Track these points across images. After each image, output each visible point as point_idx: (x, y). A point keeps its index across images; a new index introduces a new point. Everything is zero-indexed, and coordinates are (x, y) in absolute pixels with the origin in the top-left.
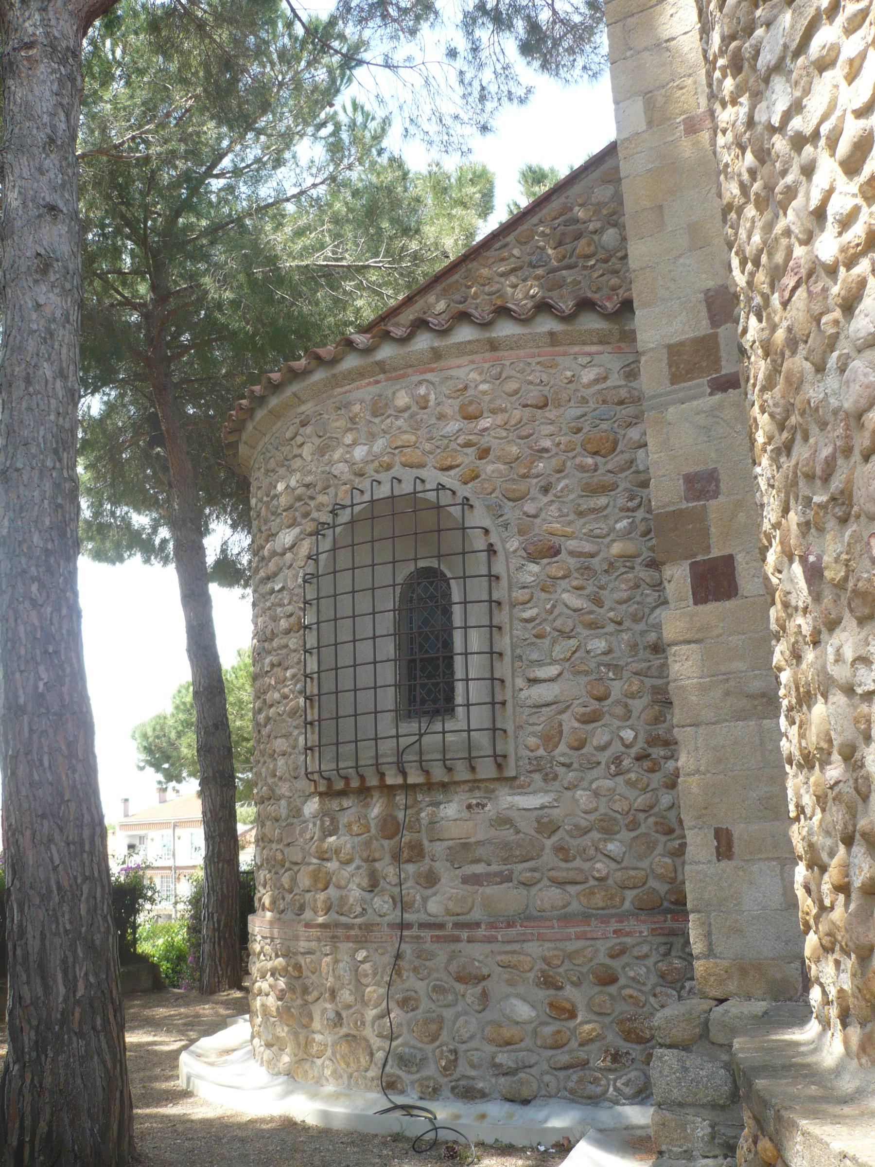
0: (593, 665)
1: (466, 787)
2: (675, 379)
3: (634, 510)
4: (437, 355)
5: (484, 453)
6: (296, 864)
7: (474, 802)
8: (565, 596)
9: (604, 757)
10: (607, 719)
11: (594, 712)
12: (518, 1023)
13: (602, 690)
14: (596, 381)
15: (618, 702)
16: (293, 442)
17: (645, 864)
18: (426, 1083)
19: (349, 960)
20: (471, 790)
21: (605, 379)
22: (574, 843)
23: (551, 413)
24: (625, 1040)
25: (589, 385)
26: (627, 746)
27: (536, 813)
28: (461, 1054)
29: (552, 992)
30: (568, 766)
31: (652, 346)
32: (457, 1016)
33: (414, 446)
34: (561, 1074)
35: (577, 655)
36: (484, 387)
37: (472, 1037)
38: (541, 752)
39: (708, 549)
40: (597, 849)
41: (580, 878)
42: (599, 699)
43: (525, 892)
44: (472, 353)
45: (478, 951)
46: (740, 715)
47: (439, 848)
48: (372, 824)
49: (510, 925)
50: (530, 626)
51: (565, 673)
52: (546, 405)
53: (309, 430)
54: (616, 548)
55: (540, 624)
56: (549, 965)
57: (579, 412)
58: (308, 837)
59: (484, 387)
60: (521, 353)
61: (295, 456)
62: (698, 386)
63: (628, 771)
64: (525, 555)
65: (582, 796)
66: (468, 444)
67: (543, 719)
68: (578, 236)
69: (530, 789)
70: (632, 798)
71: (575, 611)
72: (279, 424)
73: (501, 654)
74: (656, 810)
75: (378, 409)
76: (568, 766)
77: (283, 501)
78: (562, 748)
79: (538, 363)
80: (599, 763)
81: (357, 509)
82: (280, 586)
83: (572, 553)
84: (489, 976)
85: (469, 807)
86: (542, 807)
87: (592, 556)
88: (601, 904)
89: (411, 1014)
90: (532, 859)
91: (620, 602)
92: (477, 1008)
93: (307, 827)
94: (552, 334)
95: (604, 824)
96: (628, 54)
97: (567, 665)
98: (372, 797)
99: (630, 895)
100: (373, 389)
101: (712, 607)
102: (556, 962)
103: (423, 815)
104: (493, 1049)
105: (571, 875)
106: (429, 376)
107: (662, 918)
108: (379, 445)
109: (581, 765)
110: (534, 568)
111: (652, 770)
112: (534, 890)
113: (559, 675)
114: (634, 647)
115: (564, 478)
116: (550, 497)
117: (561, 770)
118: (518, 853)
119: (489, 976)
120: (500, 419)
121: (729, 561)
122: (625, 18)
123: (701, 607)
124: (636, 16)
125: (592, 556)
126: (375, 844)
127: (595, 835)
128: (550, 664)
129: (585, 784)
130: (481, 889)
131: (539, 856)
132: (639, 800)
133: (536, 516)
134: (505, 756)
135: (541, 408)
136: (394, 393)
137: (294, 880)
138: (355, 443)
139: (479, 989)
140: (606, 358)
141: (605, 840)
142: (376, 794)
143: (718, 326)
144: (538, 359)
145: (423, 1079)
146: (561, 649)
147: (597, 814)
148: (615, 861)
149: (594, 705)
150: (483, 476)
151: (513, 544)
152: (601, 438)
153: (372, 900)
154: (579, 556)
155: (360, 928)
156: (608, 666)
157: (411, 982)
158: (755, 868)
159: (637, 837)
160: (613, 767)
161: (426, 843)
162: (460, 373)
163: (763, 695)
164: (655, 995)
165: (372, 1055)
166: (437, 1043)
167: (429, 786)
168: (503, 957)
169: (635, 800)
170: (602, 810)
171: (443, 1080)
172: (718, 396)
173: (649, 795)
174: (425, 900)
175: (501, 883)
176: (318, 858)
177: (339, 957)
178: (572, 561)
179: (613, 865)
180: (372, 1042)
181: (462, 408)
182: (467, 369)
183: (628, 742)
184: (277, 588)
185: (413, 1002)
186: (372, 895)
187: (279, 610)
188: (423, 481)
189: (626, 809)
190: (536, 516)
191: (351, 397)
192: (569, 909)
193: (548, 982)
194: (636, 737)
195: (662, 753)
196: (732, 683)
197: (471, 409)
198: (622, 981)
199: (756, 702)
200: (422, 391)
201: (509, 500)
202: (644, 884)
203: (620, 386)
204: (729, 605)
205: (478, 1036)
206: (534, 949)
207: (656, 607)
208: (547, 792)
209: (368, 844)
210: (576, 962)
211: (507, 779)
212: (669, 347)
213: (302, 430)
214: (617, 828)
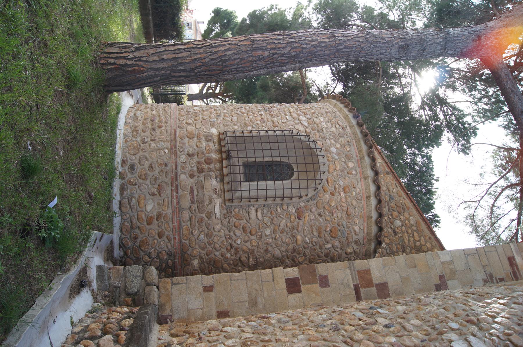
0: (261, 230)
1: (222, 188)
2: (359, 272)
3: (312, 243)
4: (366, 178)
5: (332, 194)
6: (195, 125)
7: (217, 191)
8: (284, 221)
9: (232, 234)
10: (244, 234)
11: (246, 231)
12: (145, 206)
13: (254, 233)
14: (355, 231)
15: (249, 238)
16: (337, 124)
17: (197, 247)
18: (125, 174)
19: (164, 147)
20: (221, 190)
21: (355, 234)
22: (204, 224)
23: (344, 215)
24: (140, 241)
25: (353, 229)
26: (235, 242)
27: (213, 211)
28: (135, 186)
29: (156, 217)
30: (229, 222)
31: (370, 264)
32: (147, 185)
33: (335, 169)
34: (129, 220)
35: (265, 225)
36: (354, 193)
37: (140, 190)
38: (233, 213)
39: (303, 283)
40: (202, 231)
41: (192, 226)
42: (250, 232)
43: (188, 208)
44: (366, 190)
45: (169, 192)
46: (250, 295)
47: (202, 178)
48: (210, 155)
49: (177, 203)
50: (275, 209)
51: (259, 221)
52: (347, 215)
53: (341, 130)
54: (299, 237)
55: (275, 213)
56: (164, 216)
57: (345, 226)
58: (205, 130)
59: (354, 193)
60: (365, 207)
61: (332, 125)
62: (356, 280)
63: (227, 242)
64: (298, 208)
65: (218, 227)
66: (335, 188)
67: (244, 214)
68: (399, 213)
69: (221, 210)
70: (218, 243)
71: (279, 224)
72: (343, 118)
73: (266, 200)
74: (214, 250)
75: (349, 157)
76: (229, 222)
77: (317, 120)
78: (234, 220)
79: (361, 212)
80: (230, 232)
81: (315, 150)
82: (288, 118)
83: (298, 223)
84: (161, 196)
85: (215, 189)
86: (215, 214)
87: (297, 230)
88: (184, 233)
89: (147, 169)
90: (198, 210)
91: (282, 239)
92: (150, 192)
93: (208, 130)
94: (371, 217)
95: (210, 234)
96: (466, 255)
97: (262, 222)
98: (218, 154)
99: (187, 242)
100: (354, 156)
101: (284, 285)
102: (165, 218)
103: (213, 173)
104: (137, 198)
105: (193, 223)
106: (359, 174)
107: (179, 253)
108: (335, 156)
109: (229, 226)
110: (294, 211)
111: (227, 249)
112: (188, 211)
113: (259, 219)
114: (268, 244)
115: (323, 220)
116: (317, 216)
117: (228, 220)
118: (200, 205)
119: (161, 196)
120: (344, 200)
121: (300, 291)
122: (478, 254)
123: (284, 281)
124: (478, 258)
125: (297, 230)
126: (203, 156)
127: (206, 230)
128: (262, 216)
129: (223, 228)
130: (188, 193)
131: (199, 212)
132: (218, 245)
133: (311, 211)
134: (232, 202)
135: (347, 213)
136: (353, 162)
137: (190, 124)
138: (337, 148)
139: (156, 193)
140: (362, 234)
141: (204, 234)
142: (219, 156)
143: (376, 287)
144: (363, 212)
145: (126, 173)
146: (267, 220)
147: (213, 231)
148: (198, 237)
149: (248, 230)
150: (325, 194)
151: (302, 204)
152: (336, 233)
153: (184, 154)
154: (297, 226)
155: (175, 151)
156: (261, 235)
157: (157, 170)
158: (201, 299)
159: (206, 244)
160: (228, 237)
161: (203, 174)
162: (359, 186)
163: (256, 303)
164: (155, 250)
165: (134, 155)
166: (138, 178)
167: (222, 176)
168: (167, 201)
169: (218, 244)
170: (214, 233)
171: (126, 180)
172: (353, 287)
173: (219, 248)
174: (185, 173)
175: (191, 200)
176: (198, 134)
177: (165, 143)
178: (295, 223)
179: (196, 237)
180: (138, 155)
181: (348, 186)
182: (360, 187)
183: (236, 242)
184: (287, 117)
185: (151, 170)
186: (186, 155)
187: (280, 117)
188: (324, 173)
189: (215, 241)
190: (311, 211)
191: (352, 147)
192: (182, 222)
193: (159, 216)
194: (238, 244)
195: (232, 252)
196: (260, 292)
197: (347, 190)
198: (159, 240)
199: (254, 300)
200: (354, 172)
201: (317, 202)
202: (190, 247)
203: (352, 239)
204: (285, 291)
205: (141, 192)
206: (169, 211)
207: (280, 250)
208: (220, 215)
209: (203, 153)
210: (165, 225)
211: (225, 202)
212: (370, 270)
213: (341, 127)
214: (208, 238)
